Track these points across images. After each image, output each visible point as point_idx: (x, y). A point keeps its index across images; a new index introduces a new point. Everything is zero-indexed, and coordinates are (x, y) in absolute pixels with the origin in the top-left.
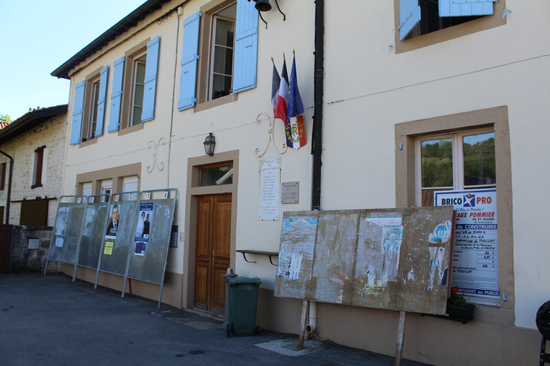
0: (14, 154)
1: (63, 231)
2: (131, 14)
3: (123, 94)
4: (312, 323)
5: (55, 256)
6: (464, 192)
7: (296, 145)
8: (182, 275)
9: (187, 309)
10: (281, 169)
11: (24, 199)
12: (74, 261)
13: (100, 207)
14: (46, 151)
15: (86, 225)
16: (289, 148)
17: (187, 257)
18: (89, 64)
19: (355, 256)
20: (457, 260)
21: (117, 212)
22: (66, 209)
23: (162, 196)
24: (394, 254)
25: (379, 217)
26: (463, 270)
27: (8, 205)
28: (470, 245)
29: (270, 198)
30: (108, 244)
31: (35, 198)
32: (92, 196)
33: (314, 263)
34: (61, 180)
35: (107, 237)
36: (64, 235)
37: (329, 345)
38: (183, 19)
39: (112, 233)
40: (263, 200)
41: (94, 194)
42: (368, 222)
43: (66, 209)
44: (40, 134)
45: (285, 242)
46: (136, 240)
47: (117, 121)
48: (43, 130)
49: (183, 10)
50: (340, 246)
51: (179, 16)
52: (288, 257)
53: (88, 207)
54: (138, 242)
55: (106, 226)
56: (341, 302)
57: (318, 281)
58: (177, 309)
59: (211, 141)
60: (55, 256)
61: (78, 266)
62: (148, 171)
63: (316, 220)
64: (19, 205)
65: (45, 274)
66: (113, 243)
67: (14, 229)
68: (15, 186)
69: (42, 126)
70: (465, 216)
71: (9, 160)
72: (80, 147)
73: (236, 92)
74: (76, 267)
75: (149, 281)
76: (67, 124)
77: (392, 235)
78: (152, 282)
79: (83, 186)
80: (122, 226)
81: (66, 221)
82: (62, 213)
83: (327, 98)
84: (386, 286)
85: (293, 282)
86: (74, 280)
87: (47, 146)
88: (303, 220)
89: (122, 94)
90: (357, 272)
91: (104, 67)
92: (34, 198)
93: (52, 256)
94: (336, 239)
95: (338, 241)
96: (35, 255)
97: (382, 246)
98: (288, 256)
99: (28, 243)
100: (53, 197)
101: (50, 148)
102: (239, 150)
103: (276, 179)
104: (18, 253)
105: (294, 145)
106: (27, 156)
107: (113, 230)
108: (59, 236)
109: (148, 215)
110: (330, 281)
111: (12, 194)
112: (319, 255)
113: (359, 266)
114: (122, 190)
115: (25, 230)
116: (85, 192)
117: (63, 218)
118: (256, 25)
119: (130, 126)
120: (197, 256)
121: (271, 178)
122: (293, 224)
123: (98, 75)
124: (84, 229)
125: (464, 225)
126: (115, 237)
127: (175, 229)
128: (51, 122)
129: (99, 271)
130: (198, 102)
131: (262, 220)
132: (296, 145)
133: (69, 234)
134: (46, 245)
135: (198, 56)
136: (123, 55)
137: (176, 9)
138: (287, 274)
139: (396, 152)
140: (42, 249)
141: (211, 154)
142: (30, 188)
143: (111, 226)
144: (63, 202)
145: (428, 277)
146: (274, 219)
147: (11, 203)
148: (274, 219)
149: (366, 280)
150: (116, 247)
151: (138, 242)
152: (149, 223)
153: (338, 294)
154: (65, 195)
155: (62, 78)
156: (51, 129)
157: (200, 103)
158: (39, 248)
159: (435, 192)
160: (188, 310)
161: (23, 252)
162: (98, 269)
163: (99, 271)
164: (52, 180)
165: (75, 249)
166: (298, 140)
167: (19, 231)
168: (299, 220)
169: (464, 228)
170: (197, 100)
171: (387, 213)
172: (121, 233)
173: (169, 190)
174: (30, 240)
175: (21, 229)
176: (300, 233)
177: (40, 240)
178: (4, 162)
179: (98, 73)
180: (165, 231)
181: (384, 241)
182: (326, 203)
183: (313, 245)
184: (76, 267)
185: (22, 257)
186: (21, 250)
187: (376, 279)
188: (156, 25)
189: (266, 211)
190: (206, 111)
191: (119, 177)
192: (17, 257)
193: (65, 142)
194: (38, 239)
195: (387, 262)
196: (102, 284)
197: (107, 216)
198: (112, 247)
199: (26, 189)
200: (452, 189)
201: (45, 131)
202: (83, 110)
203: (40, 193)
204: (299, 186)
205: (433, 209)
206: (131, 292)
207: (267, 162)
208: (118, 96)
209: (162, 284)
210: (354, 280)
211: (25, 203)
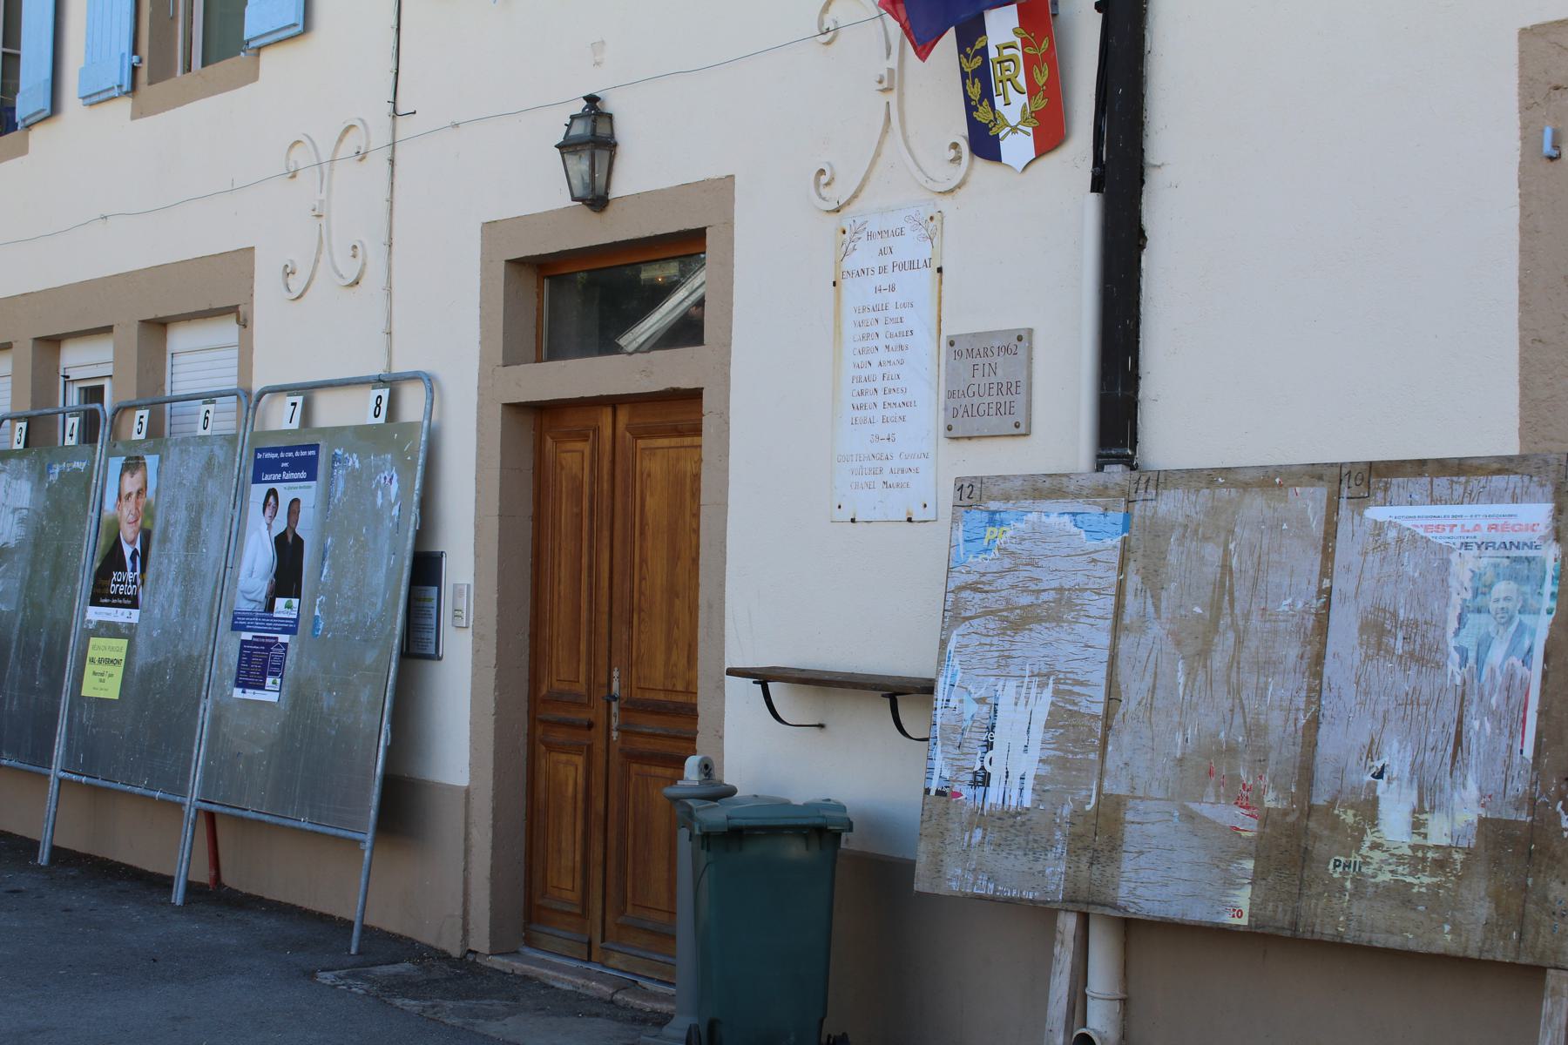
10: (940, 270)
13: (57, 469)
21: (141, 492)
23: (358, 410)
25: (1434, 502)
29: (889, 413)
33: (1107, 727)
35: (95, 614)
40: (854, 422)
41: (26, 408)
42: (1379, 527)
45: (963, 629)
46: (236, 627)
47: (126, 46)
50: (1239, 642)
52: (981, 701)
54: (247, 636)
56: (1244, 921)
57: (1129, 817)
63: (1117, 516)
66: (124, 643)
72: (137, 114)
75: (304, 824)
80: (167, 561)
86: (43, 857)
88: (1054, 517)
90: (1324, 772)
94: (1216, 608)
95: (1225, 621)
103: (920, 320)
110: (1190, 817)
112: (1134, 688)
113: (1333, 743)
114: (161, 385)
121: (893, 313)
131: (853, 521)
132: (1017, 146)
138: (974, 784)
141: (596, 200)
143: (112, 560)
148: (908, 513)
149: (1369, 810)
151: (247, 636)
152: (298, 542)
160: (498, 962)
162: (56, 771)
166: (1024, 121)
171: (1476, 482)
173: (392, 383)
180: (379, 578)
181: (1460, 618)
183: (1104, 639)
189: (871, 478)
191: (143, 321)
196: (75, 840)
204: (1030, 349)
206: (217, 877)
207: (870, 236)
210: (1310, 811)
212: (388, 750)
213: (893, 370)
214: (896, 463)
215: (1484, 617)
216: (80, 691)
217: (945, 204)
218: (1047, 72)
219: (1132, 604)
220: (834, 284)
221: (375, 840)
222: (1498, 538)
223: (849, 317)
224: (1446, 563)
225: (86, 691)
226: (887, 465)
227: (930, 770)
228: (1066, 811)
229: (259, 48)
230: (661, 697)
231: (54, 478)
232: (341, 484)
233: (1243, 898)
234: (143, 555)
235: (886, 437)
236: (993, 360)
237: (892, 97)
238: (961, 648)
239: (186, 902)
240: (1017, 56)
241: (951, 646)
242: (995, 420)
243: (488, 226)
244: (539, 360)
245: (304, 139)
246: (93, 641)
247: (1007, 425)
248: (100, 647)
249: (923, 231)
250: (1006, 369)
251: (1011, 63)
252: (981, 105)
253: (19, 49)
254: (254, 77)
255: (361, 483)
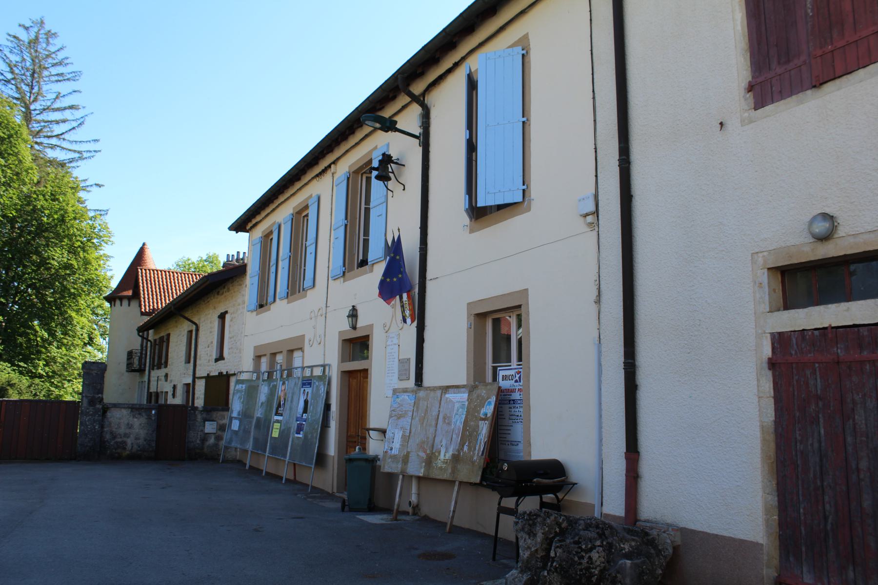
0: (199, 319)
1: (239, 412)
2: (289, 171)
3: (292, 255)
4: (414, 499)
5: (231, 441)
6: (515, 369)
7: (409, 320)
9: (337, 492)
11: (208, 374)
12: (248, 447)
13: (272, 384)
14: (228, 317)
15: (260, 404)
16: (405, 324)
17: (337, 438)
18: (263, 219)
19: (436, 430)
20: (509, 434)
21: (285, 390)
22: (242, 387)
23: (318, 372)
24: (459, 429)
25: (454, 393)
26: (513, 443)
27: (194, 381)
28: (517, 419)
30: (277, 425)
31: (217, 374)
32: (266, 372)
33: (409, 438)
34: (240, 352)
35: (276, 418)
36: (240, 417)
37: (426, 519)
38: (336, 176)
39: (280, 414)
40: (388, 376)
41: (268, 370)
42: (447, 398)
43: (242, 387)
44: (223, 296)
45: (392, 419)
46: (297, 421)
47: (286, 288)
48: (226, 292)
49: (336, 168)
50: (427, 421)
51: (333, 174)
52: (393, 433)
53: (262, 385)
54: (298, 422)
55: (275, 405)
56: (422, 475)
57: (410, 455)
58: (329, 493)
59: (353, 314)
60: (231, 441)
61: (251, 452)
62: (384, 329)
63: (414, 396)
64: (203, 382)
65: (221, 462)
66: (279, 424)
67: (190, 410)
68: (200, 359)
69: (224, 288)
70: (515, 392)
71: (194, 327)
72: (257, 315)
73: (373, 262)
74: (249, 452)
75: (304, 464)
76: (246, 286)
77: (460, 410)
78: (308, 465)
79: (260, 360)
80: (287, 406)
81: (242, 400)
82: (238, 391)
83: (430, 275)
84: (450, 458)
85: (394, 458)
86: (247, 467)
87: (228, 312)
88: (405, 396)
89: (290, 256)
90: (435, 445)
91: (313, 196)
92: (217, 374)
93: (228, 440)
94: (425, 415)
95: (426, 417)
96: (212, 441)
97: (453, 420)
98: (393, 432)
99: (204, 426)
100: (233, 372)
101: (231, 314)
102: (526, 290)
103: (396, 355)
104: (194, 438)
106: (211, 323)
107: (281, 410)
108: (236, 418)
109: (308, 392)
110: (418, 455)
111: (198, 368)
112: (413, 430)
113: (437, 440)
114: (292, 366)
115: (201, 411)
116: (295, 363)
117: (239, 398)
118: (385, 194)
119: (299, 292)
120: (348, 437)
122: (398, 400)
123: (307, 207)
124: (258, 410)
125: (514, 400)
126: (282, 417)
127: (327, 407)
128: (232, 283)
129: (268, 456)
130: (346, 271)
133: (245, 415)
134: (222, 428)
135: (346, 221)
136: (291, 212)
137: (329, 166)
138: (390, 450)
139: (467, 329)
140: (219, 433)
141: (354, 328)
142: (214, 361)
143: (279, 406)
144: (241, 378)
145: (475, 449)
147: (196, 380)
149: (439, 453)
150: (283, 428)
151: (298, 422)
152: (308, 401)
153: (421, 468)
154: (244, 370)
155: (241, 232)
156: (232, 291)
157: (348, 272)
158: (217, 431)
159: (499, 368)
160: (337, 494)
161: (199, 437)
162: (267, 454)
163: (268, 456)
164: (233, 352)
165: (250, 432)
167: (195, 412)
168: (403, 396)
169: (514, 403)
170: (345, 269)
171: (460, 390)
172: (286, 413)
173: (324, 366)
174: (206, 422)
175: (197, 410)
176: (402, 409)
177: (217, 423)
178: (190, 329)
179: (270, 230)
180: (319, 410)
181: (455, 416)
182: (428, 381)
183: (410, 421)
184: (249, 452)
185: (198, 442)
186: (198, 433)
187: (445, 452)
188: (315, 181)
190: (352, 281)
191: (288, 350)
192: (193, 442)
193: (244, 307)
194: (215, 421)
195: (454, 436)
196: (272, 470)
197: (277, 395)
199: (211, 363)
200: (510, 366)
201: (228, 293)
202: (259, 271)
203: (223, 367)
204: (410, 362)
205: (486, 386)
206: (295, 478)
208: (286, 259)
209: (313, 466)
210: (432, 453)
211: (208, 378)
212: (318, 447)
215: (457, 416)
217: (400, 331)
219: (414, 415)
221: (314, 467)
222: (461, 400)
224: (454, 405)
225: (273, 436)
227: (384, 447)
228: (402, 455)
229: (373, 264)
231: (271, 386)
232: (315, 388)
233: (422, 470)
234: (284, 404)
237: (394, 309)
238: (391, 422)
239: (285, 483)
241: (390, 422)
243: (340, 332)
244: (350, 361)
246: (275, 424)
248: (277, 425)
253: (369, 236)
254: (306, 296)
255: (318, 388)
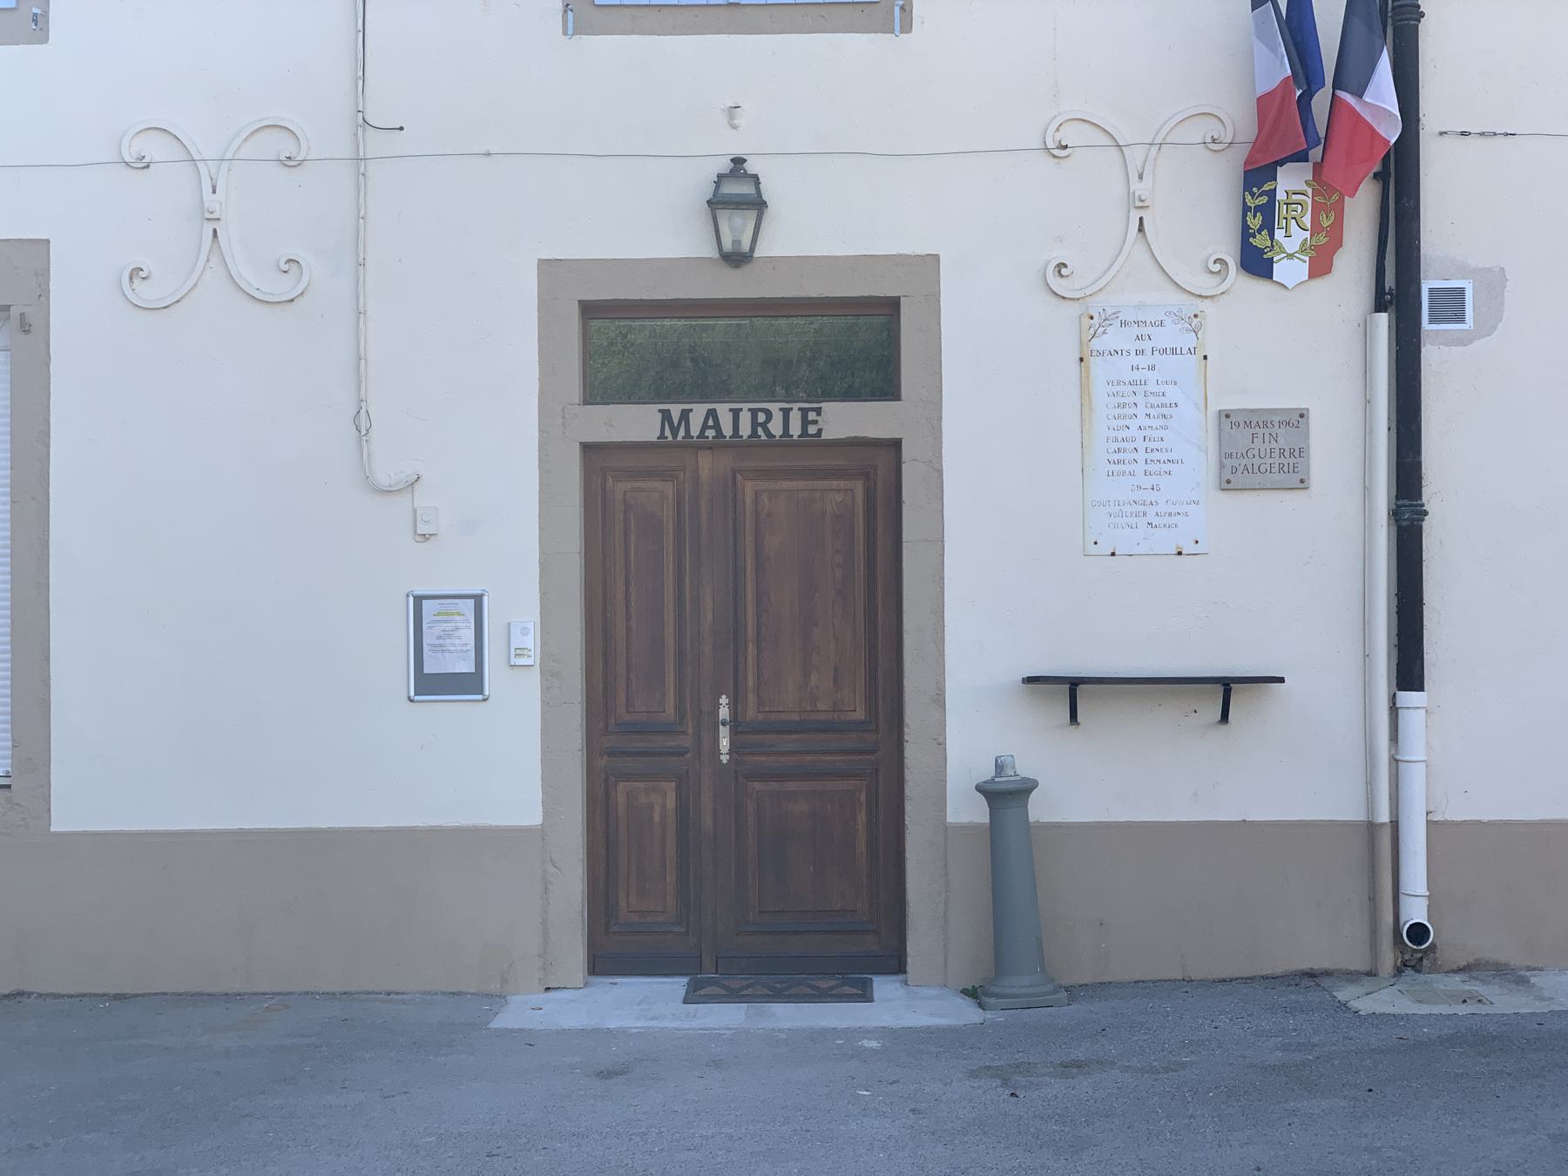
8: (541, 832)
10: (1205, 357)
105: (1277, 269)
121: (1152, 387)
131: (1113, 554)
132: (1290, 270)
146: (1178, 548)
148: (1178, 548)
166: (1303, 250)
189: (1133, 520)
198: (537, 668)
207: (1124, 324)
213: (1158, 434)
214: (1162, 508)
216: (1028, 819)
218: (1333, 218)
220: (1081, 360)
223: (1100, 389)
226: (1151, 511)
230: (795, 717)
235: (1151, 486)
236: (1274, 431)
240: (1307, 202)
242: (1277, 476)
245: (155, 148)
247: (1293, 479)
249: (1187, 325)
250: (1285, 439)
251: (1299, 206)
252: (1260, 233)
